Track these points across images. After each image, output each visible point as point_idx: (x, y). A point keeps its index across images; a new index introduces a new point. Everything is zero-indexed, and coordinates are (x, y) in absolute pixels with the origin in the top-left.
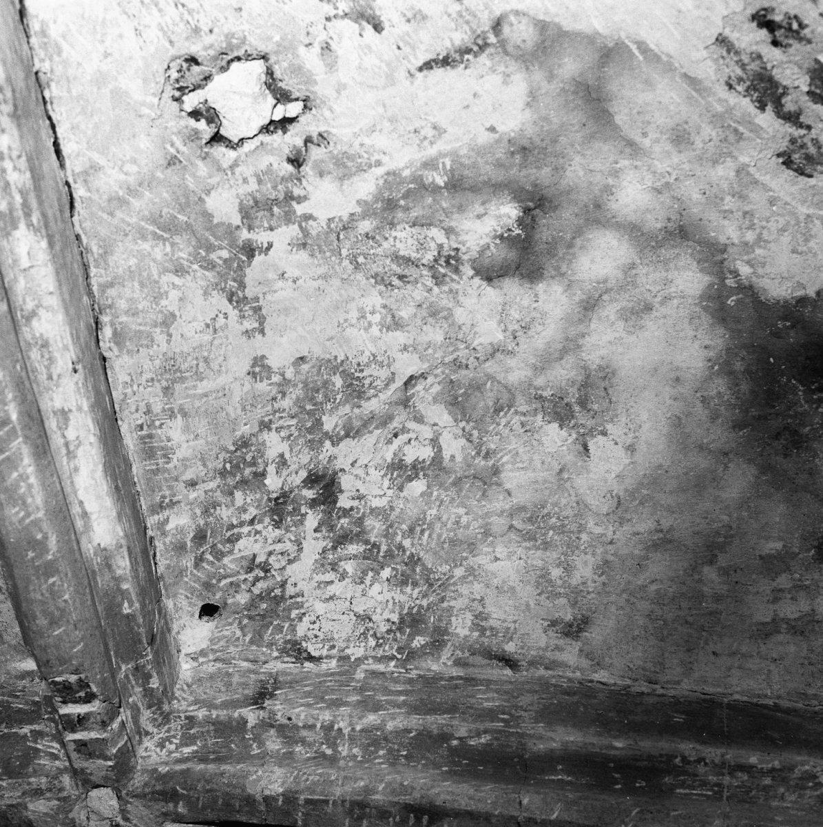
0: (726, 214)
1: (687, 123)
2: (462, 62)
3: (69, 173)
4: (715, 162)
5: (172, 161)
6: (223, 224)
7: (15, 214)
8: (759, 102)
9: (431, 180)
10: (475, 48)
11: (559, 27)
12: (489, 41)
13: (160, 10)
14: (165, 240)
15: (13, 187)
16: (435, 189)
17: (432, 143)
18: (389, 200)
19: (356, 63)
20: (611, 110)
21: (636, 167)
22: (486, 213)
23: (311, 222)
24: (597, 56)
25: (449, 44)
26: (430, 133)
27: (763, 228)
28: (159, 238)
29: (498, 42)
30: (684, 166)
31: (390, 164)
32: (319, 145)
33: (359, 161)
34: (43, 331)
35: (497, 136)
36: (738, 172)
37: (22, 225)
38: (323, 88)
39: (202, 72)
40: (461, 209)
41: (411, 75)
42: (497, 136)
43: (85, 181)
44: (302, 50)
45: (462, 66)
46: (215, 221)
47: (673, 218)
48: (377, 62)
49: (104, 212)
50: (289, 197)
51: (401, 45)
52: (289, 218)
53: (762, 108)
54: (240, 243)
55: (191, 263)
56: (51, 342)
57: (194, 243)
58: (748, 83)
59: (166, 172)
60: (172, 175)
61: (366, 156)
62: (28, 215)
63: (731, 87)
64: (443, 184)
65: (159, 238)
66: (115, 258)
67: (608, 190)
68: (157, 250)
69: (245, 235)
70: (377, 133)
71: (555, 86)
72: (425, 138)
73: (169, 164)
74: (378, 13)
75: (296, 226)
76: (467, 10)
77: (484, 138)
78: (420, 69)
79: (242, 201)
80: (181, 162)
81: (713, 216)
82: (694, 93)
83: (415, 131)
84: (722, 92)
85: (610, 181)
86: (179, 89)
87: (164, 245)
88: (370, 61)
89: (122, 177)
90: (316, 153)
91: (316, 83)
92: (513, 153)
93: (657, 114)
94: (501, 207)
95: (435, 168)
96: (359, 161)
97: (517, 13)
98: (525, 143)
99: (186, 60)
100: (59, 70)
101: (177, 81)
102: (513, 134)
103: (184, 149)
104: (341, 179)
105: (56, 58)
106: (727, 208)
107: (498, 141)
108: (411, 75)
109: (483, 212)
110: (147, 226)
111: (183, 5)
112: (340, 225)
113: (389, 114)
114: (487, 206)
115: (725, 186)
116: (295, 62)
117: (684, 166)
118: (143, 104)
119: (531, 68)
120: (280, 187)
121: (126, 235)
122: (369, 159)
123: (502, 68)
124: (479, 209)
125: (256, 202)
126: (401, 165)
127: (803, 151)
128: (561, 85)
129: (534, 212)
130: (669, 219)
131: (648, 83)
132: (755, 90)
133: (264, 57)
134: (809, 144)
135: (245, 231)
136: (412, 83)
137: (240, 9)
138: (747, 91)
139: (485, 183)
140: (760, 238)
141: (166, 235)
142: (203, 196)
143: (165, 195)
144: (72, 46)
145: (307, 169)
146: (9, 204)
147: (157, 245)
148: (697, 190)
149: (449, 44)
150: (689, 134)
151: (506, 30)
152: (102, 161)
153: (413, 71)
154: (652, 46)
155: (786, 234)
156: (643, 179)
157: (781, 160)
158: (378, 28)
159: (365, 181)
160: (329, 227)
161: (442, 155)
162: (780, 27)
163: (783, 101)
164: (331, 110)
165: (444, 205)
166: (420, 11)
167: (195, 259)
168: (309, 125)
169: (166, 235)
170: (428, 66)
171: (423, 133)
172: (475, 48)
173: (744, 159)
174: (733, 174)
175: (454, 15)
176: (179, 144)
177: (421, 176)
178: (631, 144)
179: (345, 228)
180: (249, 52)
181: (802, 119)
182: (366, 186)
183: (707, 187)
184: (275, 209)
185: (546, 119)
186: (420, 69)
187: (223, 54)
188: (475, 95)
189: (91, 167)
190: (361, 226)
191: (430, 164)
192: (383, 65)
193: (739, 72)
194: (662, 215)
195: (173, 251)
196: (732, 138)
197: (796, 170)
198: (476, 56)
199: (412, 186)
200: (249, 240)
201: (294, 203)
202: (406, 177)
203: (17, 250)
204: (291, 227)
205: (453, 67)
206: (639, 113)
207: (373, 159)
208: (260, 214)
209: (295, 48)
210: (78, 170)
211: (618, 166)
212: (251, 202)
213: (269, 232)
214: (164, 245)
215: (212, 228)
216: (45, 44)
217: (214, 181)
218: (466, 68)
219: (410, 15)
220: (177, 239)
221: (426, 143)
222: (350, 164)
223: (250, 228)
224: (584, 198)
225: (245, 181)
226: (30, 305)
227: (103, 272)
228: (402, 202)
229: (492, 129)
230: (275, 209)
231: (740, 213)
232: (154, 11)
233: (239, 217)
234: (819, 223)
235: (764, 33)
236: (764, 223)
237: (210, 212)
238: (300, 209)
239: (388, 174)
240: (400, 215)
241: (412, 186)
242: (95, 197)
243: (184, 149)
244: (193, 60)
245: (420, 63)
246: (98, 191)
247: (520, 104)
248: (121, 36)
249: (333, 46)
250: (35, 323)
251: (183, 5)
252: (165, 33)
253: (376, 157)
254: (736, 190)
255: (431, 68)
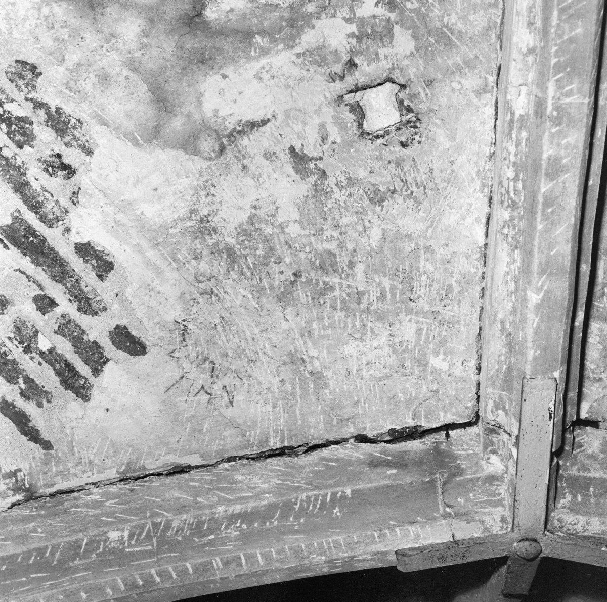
0: (65, 25)
1: (102, 91)
2: (243, 125)
3: (494, 95)
4: (79, 64)
5: (430, 83)
6: (406, 28)
7: (519, 125)
8: (60, 114)
9: (264, 40)
10: (235, 134)
11: (186, 153)
12: (227, 139)
13: (416, 181)
14: (446, 27)
15: (514, 143)
16: (261, 32)
17: (263, 68)
18: (293, 27)
19: (307, 127)
20: (150, 94)
21: (130, 52)
22: (227, 12)
23: (347, 16)
24: (161, 133)
25: (251, 137)
26: (266, 76)
27: (38, 19)
28: (450, 29)
29: (221, 139)
30: (99, 58)
31: (289, 55)
32: (335, 73)
33: (311, 59)
34: (528, 36)
35: (222, 72)
36: (64, 59)
37: (517, 116)
38: (328, 113)
39: (400, 135)
40: (244, 16)
41: (274, 116)
42: (222, 72)
43: (486, 86)
44: (339, 140)
45: (243, 122)
46: (411, 31)
47: (99, 16)
48: (295, 127)
49: (481, 61)
50: (359, 38)
51: (279, 138)
52: (362, 22)
53: (58, 109)
54: (397, 11)
55: (433, 4)
56: (525, 24)
57: (428, 19)
58: (69, 126)
59: (435, 77)
60: (432, 73)
61: (306, 62)
62: (512, 121)
63: (79, 121)
64: (257, 36)
65: (450, 29)
66: (483, 24)
67: (146, 34)
68: (453, 21)
69: (393, 16)
70: (297, 78)
71: (186, 110)
72: (267, 72)
73: (432, 82)
74: (292, 159)
75: (357, 15)
76: (240, 160)
77: (229, 70)
78: (268, 120)
79: (391, 43)
80: (424, 81)
81: (75, 22)
82: (100, 113)
83: (273, 77)
84: (84, 117)
85: (145, 40)
86: (415, 127)
87: (448, 23)
88: (298, 128)
89: (463, 81)
90: (338, 68)
91: (332, 117)
92: (211, 59)
93: (121, 95)
94: (217, 17)
95: (261, 49)
96: (311, 59)
97: (210, 159)
98: (203, 67)
99: (408, 146)
100: (482, 162)
101: (416, 133)
102: (211, 73)
103: (421, 90)
104: (323, 47)
105: (481, 169)
106: (66, 30)
107: (221, 68)
108: (274, 116)
109: (229, 14)
110: (456, 41)
111: (402, 181)
112: (327, 10)
113: (290, 90)
114: (227, 19)
115: (70, 47)
116: (343, 133)
117: (99, 58)
118: (438, 127)
119: (201, 122)
120: (365, 47)
121: (471, 38)
122: (305, 60)
123: (219, 120)
124: (232, 17)
125: (381, 39)
126: (283, 53)
127: (26, 81)
128: (182, 110)
129: (195, 13)
130: (102, 15)
131: (128, 116)
132: (64, 122)
133: (363, 134)
134: (23, 87)
135: (392, 19)
136: (274, 111)
137: (371, 172)
138: (69, 120)
139: (227, 36)
140: (39, 9)
141: (445, 30)
142: (415, 52)
143: (439, 60)
144: (470, 173)
145: (345, 58)
146: (520, 133)
147: (453, 24)
148: (88, 40)
149: (251, 137)
150: (99, 83)
151: (217, 147)
152: (472, 96)
153: (273, 119)
154: (130, 144)
155: (22, 17)
156: (124, 43)
157: (38, 71)
158: (292, 149)
159: (308, 43)
160: (335, 11)
161: (257, 58)
162: (58, 167)
163: (46, 116)
164: (326, 98)
165: (256, 20)
166: (267, 160)
167: (429, 7)
168: (339, 87)
169: (445, 30)
170: (264, 122)
171: (269, 76)
172: (235, 134)
173: (61, 69)
174: (67, 57)
175: (247, 156)
176: (423, 95)
177: (271, 43)
178: (135, 70)
179: (325, 8)
180: (370, 142)
181: (32, 105)
182: (308, 39)
183: (82, 44)
184: (369, 31)
185: (190, 85)
186: (268, 120)
187: (386, 145)
188: (235, 101)
189: (480, 94)
190: (314, 8)
191: (264, 52)
192: (291, 124)
193: (76, 133)
194: (107, 18)
195: (443, 16)
196: (72, 84)
197: (27, 63)
198: (235, 128)
199: (277, 36)
200: (391, 12)
201: (357, 33)
202: (281, 43)
203: (526, 101)
204: (361, 15)
205: (249, 121)
206: (133, 94)
207: (302, 59)
208: (380, 29)
209: (343, 142)
210: (488, 95)
211: (141, 52)
212: (385, 40)
213: (376, 14)
214: (448, 23)
215: (414, 27)
216: (484, 179)
217: (406, 62)
218: (241, 121)
219: (273, 157)
220: (438, 25)
221: (267, 68)
222: (317, 57)
223: (388, 20)
224: (162, 27)
225: (386, 57)
226: (530, 58)
227: (493, 18)
228: (284, 24)
229: (224, 77)
230: (369, 31)
231: (56, 27)
232: (419, 181)
233: (394, 30)
234: (103, 599)
235: (66, 160)
236: (39, 21)
237: (413, 40)
238: (353, 28)
239: (293, 47)
240: (286, 14)
241: (277, 36)
242: (483, 73)
243: (421, 90)
244: (404, 145)
245: (269, 124)
246: (480, 77)
247: (207, 96)
248: (441, 171)
249: (320, 140)
250: (531, 45)
251: (402, 181)
252: (416, 167)
253: (299, 60)
254: (62, 45)
255: (262, 121)
